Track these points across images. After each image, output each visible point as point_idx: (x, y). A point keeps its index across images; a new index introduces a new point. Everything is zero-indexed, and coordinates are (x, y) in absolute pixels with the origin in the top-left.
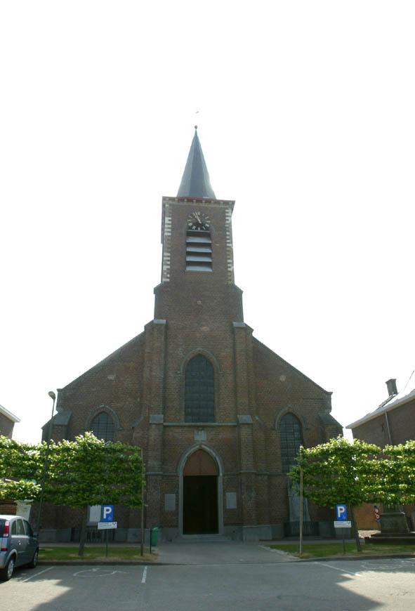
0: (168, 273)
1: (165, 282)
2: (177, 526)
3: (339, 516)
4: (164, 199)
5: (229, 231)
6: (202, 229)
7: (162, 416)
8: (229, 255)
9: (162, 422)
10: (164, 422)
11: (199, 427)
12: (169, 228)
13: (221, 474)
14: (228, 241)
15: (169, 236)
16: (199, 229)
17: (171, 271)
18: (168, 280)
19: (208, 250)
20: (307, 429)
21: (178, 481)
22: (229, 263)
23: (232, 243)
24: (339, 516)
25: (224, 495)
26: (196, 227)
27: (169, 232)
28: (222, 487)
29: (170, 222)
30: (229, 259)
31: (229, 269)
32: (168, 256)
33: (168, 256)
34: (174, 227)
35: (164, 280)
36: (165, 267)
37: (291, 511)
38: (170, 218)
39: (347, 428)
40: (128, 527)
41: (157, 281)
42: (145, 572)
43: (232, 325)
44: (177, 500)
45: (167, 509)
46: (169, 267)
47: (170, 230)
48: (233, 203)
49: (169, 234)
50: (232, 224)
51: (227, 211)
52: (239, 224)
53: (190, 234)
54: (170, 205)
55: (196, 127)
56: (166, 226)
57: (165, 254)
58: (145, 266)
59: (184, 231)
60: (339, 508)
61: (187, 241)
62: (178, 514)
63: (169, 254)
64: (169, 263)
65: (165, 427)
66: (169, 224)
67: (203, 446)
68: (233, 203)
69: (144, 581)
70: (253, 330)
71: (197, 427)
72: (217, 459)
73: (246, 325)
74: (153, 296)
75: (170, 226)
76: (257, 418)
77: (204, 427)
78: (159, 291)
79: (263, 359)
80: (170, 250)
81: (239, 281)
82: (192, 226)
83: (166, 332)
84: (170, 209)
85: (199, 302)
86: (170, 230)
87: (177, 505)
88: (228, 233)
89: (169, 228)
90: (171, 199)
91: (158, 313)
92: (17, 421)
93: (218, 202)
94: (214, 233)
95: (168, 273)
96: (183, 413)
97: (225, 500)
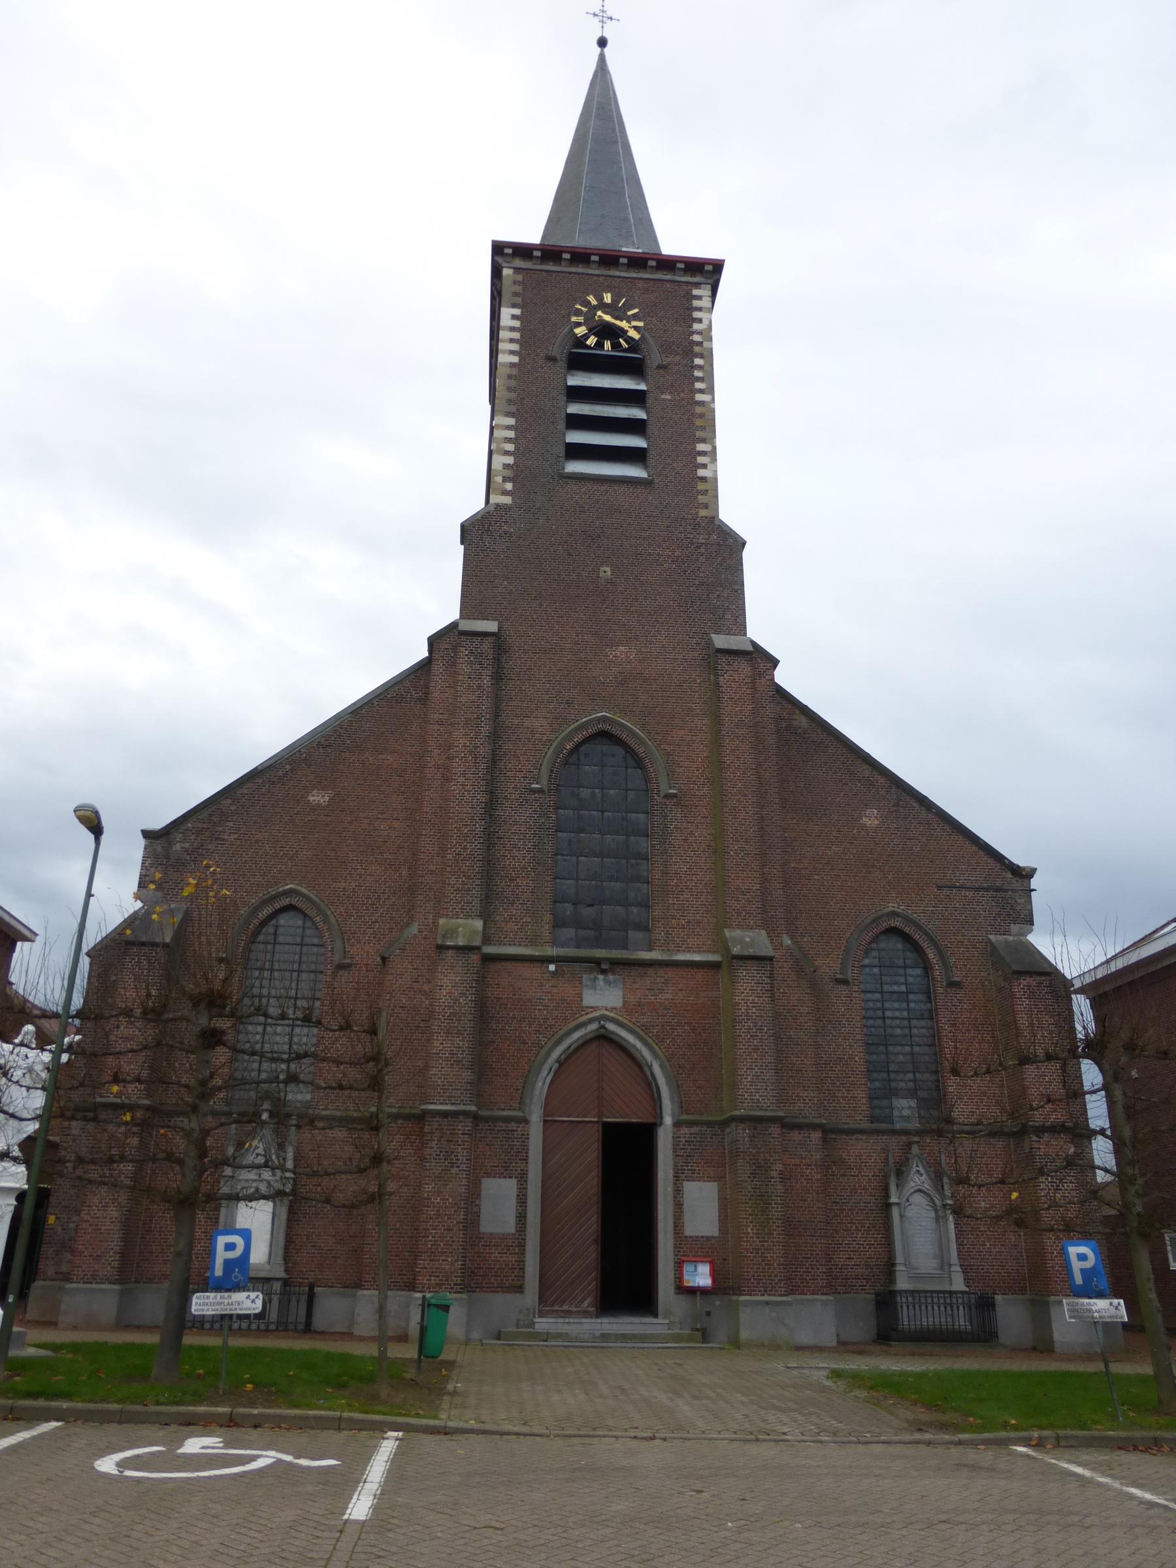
0: (505, 480)
1: (498, 506)
2: (519, 1289)
3: (219, 1271)
4: (498, 248)
5: (701, 356)
6: (616, 346)
7: (479, 924)
8: (703, 428)
9: (477, 942)
10: (487, 940)
11: (597, 962)
12: (512, 341)
13: (668, 1120)
14: (698, 385)
15: (512, 365)
16: (607, 345)
17: (516, 474)
18: (507, 500)
19: (638, 413)
20: (952, 984)
21: (525, 1137)
22: (704, 453)
23: (711, 390)
24: (219, 1271)
25: (678, 1192)
26: (600, 334)
27: (512, 352)
28: (671, 1163)
29: (517, 324)
30: (703, 441)
31: (701, 473)
32: (508, 428)
33: (508, 428)
34: (528, 340)
35: (496, 499)
36: (499, 461)
37: (899, 1259)
38: (517, 312)
39: (1081, 991)
40: (358, 1286)
41: (472, 501)
42: (377, 1470)
43: (710, 643)
44: (522, 1201)
45: (487, 1226)
46: (510, 460)
47: (515, 347)
48: (717, 267)
49: (515, 359)
50: (714, 333)
51: (696, 292)
52: (732, 328)
53: (581, 361)
54: (517, 270)
55: (602, 43)
56: (504, 334)
57: (501, 420)
58: (438, 450)
59: (558, 349)
60: (1073, 1251)
61: (569, 411)
62: (522, 1246)
63: (511, 421)
64: (510, 447)
65: (488, 959)
66: (512, 329)
67: (611, 1027)
68: (717, 267)
69: (360, 1508)
70: (775, 663)
71: (597, 965)
72: (657, 1069)
73: (754, 644)
74: (458, 552)
75: (517, 335)
76: (787, 941)
77: (617, 965)
78: (471, 532)
79: (806, 745)
80: (513, 409)
81: (732, 511)
82: (586, 337)
83: (497, 660)
84: (510, 377)
85: (606, 571)
86: (515, 347)
87: (521, 1218)
88: (698, 361)
89: (512, 341)
90: (522, 251)
91: (471, 601)
92: (25, 939)
93: (668, 264)
94: (654, 358)
95: (505, 480)
96: (548, 917)
97: (678, 1206)
